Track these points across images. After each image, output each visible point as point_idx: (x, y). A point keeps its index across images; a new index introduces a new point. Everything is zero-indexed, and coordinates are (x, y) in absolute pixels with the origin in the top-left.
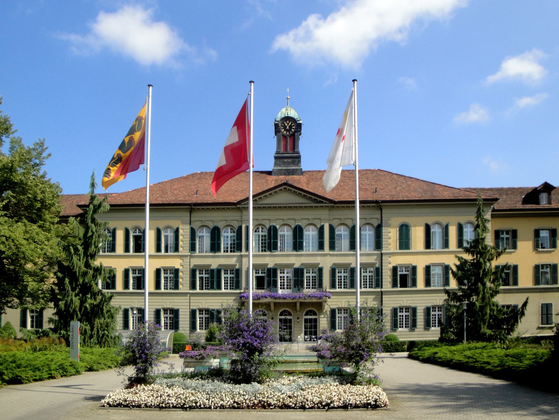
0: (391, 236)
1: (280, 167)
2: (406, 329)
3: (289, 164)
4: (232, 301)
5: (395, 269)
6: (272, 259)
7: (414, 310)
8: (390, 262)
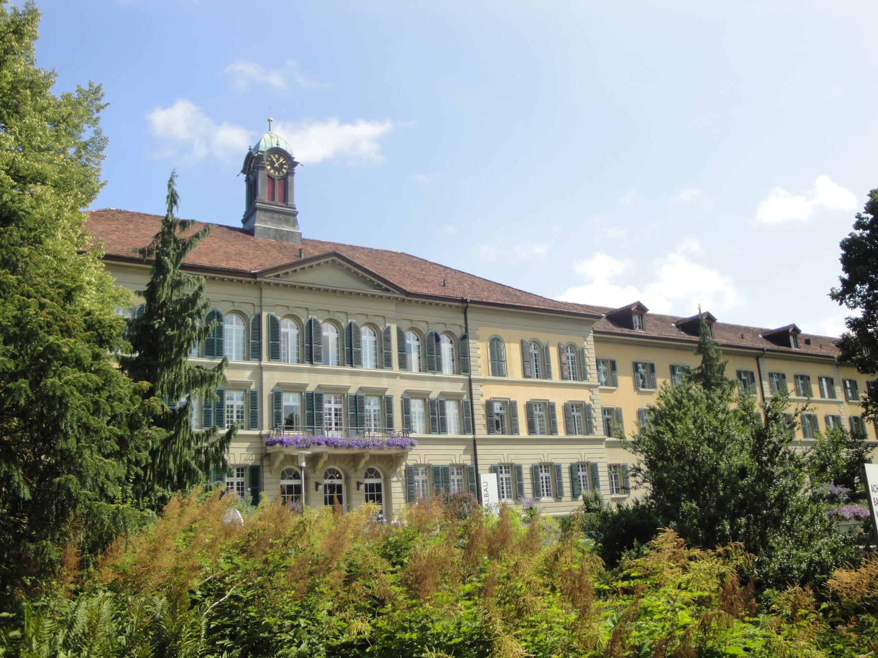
0: (479, 351)
1: (266, 224)
2: (550, 499)
3: (279, 222)
4: (244, 451)
5: (489, 405)
6: (313, 376)
7: (518, 469)
8: (484, 393)
